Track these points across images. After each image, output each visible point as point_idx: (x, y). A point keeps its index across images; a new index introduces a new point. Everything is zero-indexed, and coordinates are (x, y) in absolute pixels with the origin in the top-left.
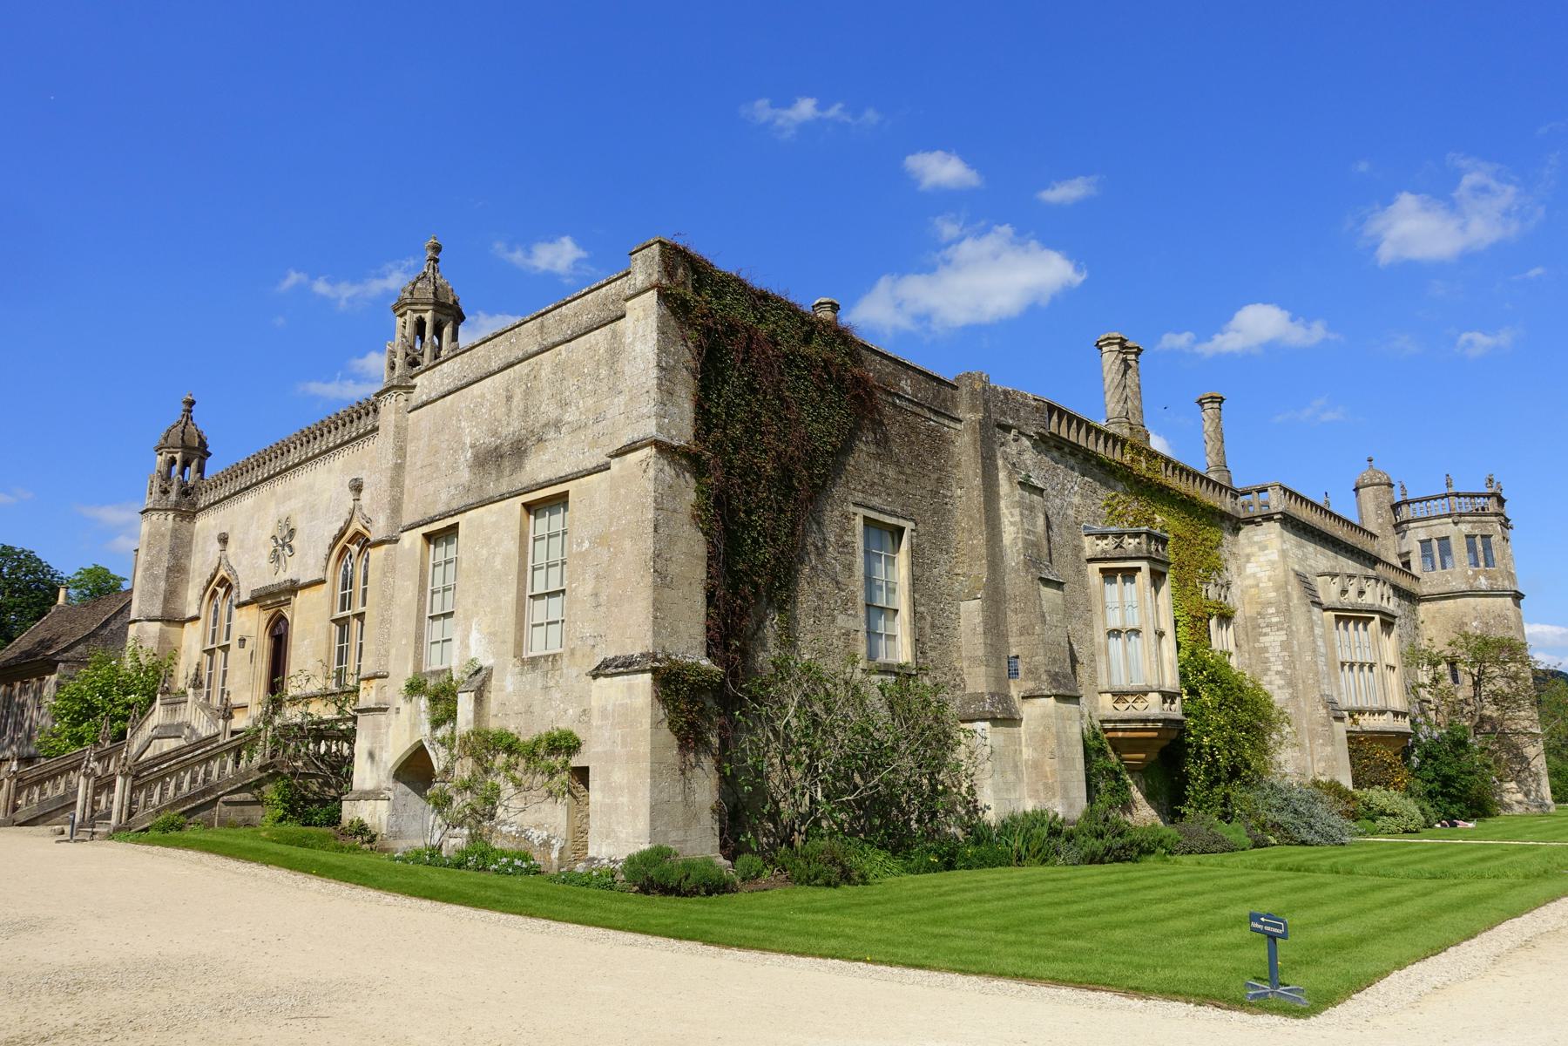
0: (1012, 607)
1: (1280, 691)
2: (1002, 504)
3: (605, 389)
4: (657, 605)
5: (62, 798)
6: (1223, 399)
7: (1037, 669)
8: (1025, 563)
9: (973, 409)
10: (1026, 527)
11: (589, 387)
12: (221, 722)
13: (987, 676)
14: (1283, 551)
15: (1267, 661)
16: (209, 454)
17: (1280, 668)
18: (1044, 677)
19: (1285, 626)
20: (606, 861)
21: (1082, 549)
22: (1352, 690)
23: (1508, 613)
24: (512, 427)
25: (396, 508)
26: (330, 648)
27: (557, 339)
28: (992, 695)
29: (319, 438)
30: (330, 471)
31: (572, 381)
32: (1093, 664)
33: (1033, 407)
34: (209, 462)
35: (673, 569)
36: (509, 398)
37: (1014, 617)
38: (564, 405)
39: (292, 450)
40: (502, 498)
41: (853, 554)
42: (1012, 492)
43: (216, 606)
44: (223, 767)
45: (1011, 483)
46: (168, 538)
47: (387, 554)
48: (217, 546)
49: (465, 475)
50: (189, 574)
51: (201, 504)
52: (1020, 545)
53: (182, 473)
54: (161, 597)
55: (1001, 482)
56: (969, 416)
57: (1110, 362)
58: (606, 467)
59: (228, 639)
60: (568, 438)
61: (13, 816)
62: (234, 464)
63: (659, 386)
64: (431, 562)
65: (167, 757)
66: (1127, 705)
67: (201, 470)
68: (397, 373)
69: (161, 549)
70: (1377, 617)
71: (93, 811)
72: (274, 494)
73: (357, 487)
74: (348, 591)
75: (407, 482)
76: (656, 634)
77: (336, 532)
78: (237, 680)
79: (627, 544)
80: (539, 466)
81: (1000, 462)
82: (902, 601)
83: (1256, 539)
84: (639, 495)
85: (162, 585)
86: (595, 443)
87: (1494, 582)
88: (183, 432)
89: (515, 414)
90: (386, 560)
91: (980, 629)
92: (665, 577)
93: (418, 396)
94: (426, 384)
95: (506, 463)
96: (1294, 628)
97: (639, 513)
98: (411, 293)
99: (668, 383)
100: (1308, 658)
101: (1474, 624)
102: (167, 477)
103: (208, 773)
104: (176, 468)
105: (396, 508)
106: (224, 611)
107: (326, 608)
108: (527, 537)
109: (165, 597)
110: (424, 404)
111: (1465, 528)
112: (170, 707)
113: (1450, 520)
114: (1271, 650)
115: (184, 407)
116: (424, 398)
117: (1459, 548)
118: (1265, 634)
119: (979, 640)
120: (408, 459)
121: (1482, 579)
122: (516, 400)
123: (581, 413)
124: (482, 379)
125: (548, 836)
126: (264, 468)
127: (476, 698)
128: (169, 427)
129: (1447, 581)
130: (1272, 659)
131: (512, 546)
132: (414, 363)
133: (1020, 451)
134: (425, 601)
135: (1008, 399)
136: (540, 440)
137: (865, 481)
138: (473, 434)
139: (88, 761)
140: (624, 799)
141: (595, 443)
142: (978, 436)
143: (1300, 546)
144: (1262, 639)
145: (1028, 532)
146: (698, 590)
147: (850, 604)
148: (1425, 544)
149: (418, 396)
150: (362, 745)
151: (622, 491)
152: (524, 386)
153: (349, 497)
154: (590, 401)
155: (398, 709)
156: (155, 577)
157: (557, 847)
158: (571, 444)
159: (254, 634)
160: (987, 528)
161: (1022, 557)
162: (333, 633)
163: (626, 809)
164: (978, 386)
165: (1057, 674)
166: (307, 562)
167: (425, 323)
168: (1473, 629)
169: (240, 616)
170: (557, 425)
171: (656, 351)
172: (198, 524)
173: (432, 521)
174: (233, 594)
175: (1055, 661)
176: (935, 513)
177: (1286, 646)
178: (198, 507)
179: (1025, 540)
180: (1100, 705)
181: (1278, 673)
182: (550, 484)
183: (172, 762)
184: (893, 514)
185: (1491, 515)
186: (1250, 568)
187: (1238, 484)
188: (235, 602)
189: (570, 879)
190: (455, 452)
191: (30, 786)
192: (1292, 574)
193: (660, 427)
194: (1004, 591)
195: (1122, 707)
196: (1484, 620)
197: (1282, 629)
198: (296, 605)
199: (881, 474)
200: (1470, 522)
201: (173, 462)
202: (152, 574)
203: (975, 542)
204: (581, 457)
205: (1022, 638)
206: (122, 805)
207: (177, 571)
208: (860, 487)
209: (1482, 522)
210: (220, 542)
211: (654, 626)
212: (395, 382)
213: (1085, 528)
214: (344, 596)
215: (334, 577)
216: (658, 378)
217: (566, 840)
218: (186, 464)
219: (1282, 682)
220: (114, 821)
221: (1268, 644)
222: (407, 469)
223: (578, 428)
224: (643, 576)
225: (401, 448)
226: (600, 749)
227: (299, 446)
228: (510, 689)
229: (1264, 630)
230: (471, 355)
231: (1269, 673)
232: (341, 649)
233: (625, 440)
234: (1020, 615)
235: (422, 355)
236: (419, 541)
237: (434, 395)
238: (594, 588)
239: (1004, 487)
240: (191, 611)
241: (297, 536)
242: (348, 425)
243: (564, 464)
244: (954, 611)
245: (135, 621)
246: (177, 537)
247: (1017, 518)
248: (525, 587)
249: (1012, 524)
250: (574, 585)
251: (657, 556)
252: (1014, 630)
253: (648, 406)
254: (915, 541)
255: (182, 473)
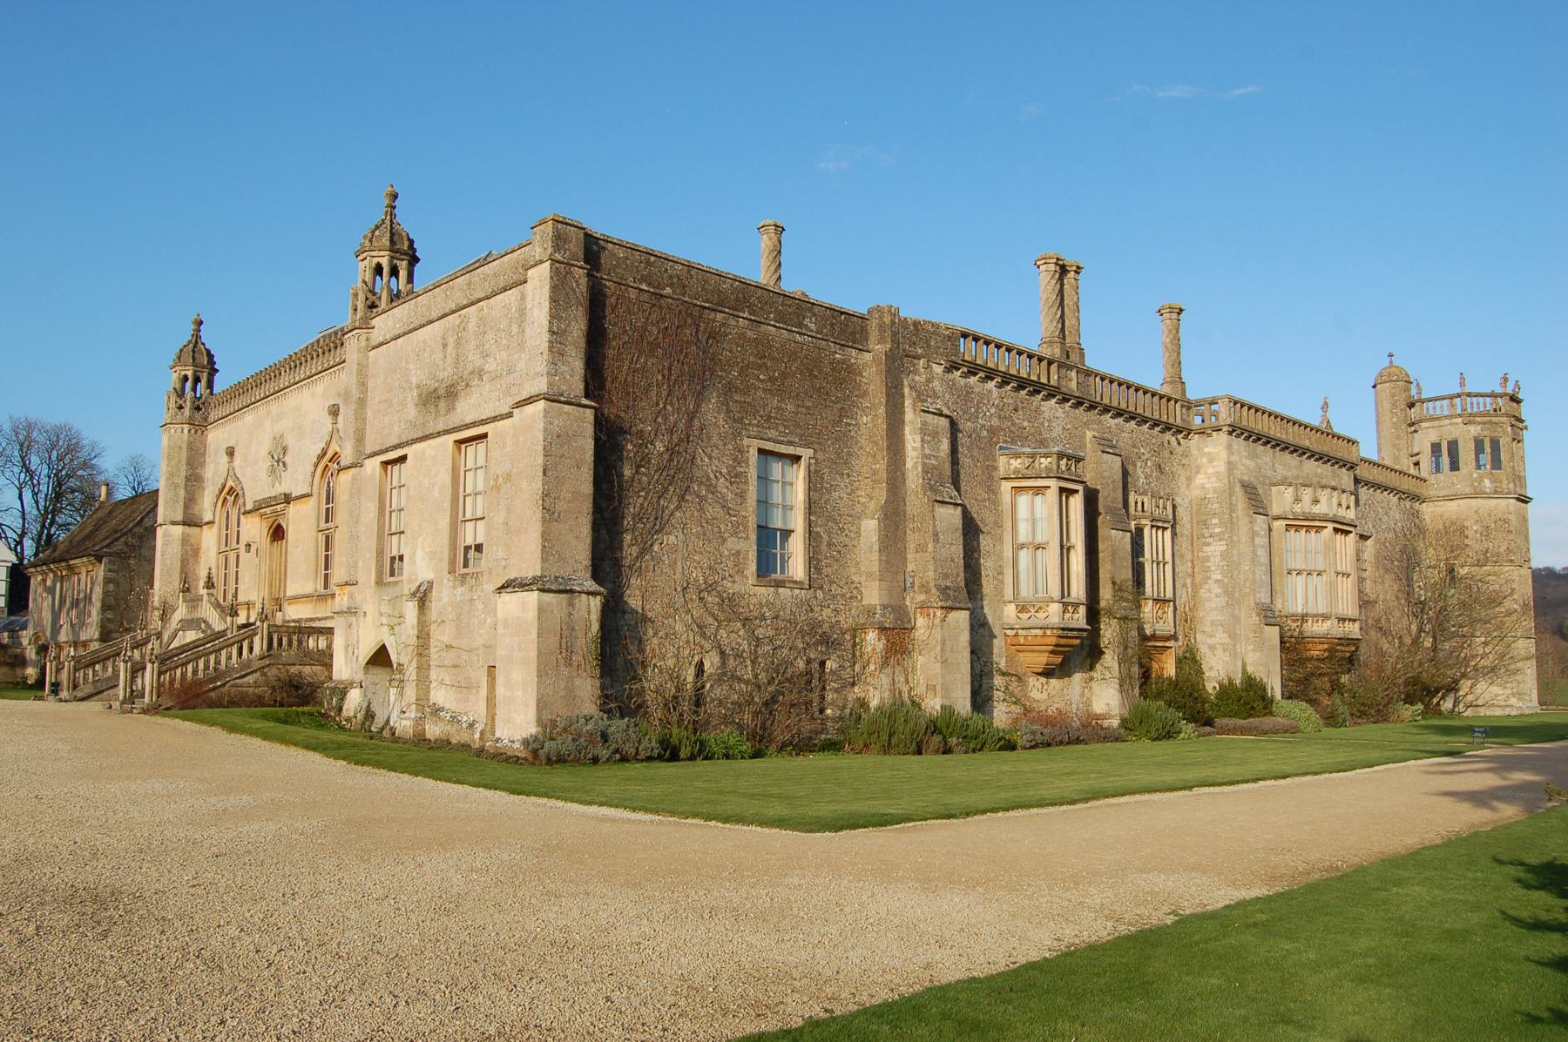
0: (911, 526)
1: (1217, 599)
2: (907, 430)
3: (516, 345)
4: (545, 537)
5: (109, 679)
6: (1181, 310)
7: (928, 583)
8: (923, 485)
9: (881, 340)
10: (927, 451)
11: (504, 342)
12: (229, 619)
13: (880, 589)
14: (1230, 463)
15: (1207, 570)
16: (217, 371)
17: (1219, 577)
18: (934, 590)
19: (1226, 536)
20: (506, 741)
21: (995, 468)
22: (1299, 596)
23: (1510, 516)
24: (447, 373)
25: (360, 439)
26: (317, 555)
27: (481, 295)
28: (885, 607)
29: (304, 364)
30: (313, 395)
31: (490, 335)
32: (1000, 577)
33: (945, 336)
34: (217, 377)
35: (561, 506)
36: (445, 346)
37: (913, 536)
38: (485, 355)
39: (283, 373)
40: (439, 434)
41: (746, 483)
42: (915, 419)
43: (228, 512)
44: (229, 658)
45: (915, 410)
46: (185, 450)
47: (354, 479)
48: (225, 458)
49: (412, 412)
50: (204, 482)
51: (211, 419)
52: (920, 469)
53: (194, 390)
54: (182, 503)
55: (906, 410)
56: (879, 347)
57: (1045, 283)
58: (510, 415)
59: (238, 543)
60: (488, 386)
61: (74, 693)
62: (245, 379)
63: (551, 349)
64: (389, 487)
65: (186, 648)
66: (1029, 614)
67: (210, 385)
68: (359, 316)
69: (180, 461)
70: (1331, 526)
71: (132, 691)
72: (269, 413)
73: (334, 412)
74: (331, 505)
75: (369, 413)
76: (544, 560)
77: (319, 452)
78: (246, 580)
79: (524, 485)
80: (469, 408)
81: (907, 390)
82: (798, 522)
83: (1206, 450)
84: (532, 443)
85: (182, 493)
86: (507, 392)
87: (1498, 485)
88: (194, 351)
89: (449, 360)
90: (352, 483)
91: (876, 547)
92: (553, 513)
93: (377, 336)
94: (384, 324)
95: (442, 404)
96: (1235, 538)
97: (532, 458)
98: (371, 241)
99: (558, 345)
100: (1247, 568)
101: (1475, 528)
102: (181, 394)
103: (218, 662)
104: (189, 385)
105: (360, 439)
106: (234, 518)
107: (313, 520)
108: (459, 470)
109: (185, 503)
110: (381, 344)
111: (1474, 430)
112: (190, 604)
113: (1460, 420)
114: (1212, 559)
115: (193, 327)
116: (381, 339)
117: (1466, 455)
118: (1208, 544)
119: (875, 556)
120: (369, 394)
121: (1487, 482)
122: (450, 348)
123: (498, 365)
124: (424, 326)
125: (474, 721)
126: (260, 389)
127: (419, 607)
128: (181, 346)
129: (1453, 483)
130: (1213, 568)
131: (445, 477)
132: (373, 306)
133: (930, 373)
134: (384, 520)
135: (918, 330)
136: (467, 385)
137: (761, 416)
138: (417, 376)
139: (126, 650)
140: (519, 693)
141: (507, 392)
142: (883, 367)
143: (1253, 456)
144: (1206, 549)
145: (929, 457)
146: (584, 522)
147: (741, 528)
148: (1436, 448)
149: (377, 336)
150: (338, 642)
151: (521, 439)
152: (456, 336)
153: (328, 420)
154: (504, 354)
155: (365, 613)
156: (177, 486)
157: (479, 729)
158: (491, 391)
159: (258, 540)
160: (888, 454)
161: (921, 480)
162: (320, 545)
163: (520, 701)
164: (887, 319)
165: (947, 587)
166: (296, 479)
167: (382, 268)
168: (1472, 532)
169: (247, 523)
170: (480, 373)
171: (548, 318)
172: (210, 437)
173: (387, 450)
174: (241, 501)
175: (946, 576)
176: (837, 439)
177: (1225, 556)
178: (209, 420)
179: (924, 465)
180: (1006, 613)
181: (1217, 581)
182: (474, 424)
183: (189, 653)
184: (790, 443)
185: (1502, 415)
186: (1200, 480)
187: (1192, 395)
188: (242, 510)
189: (481, 751)
190: (404, 390)
191: (87, 666)
192: (1238, 487)
193: (550, 385)
194: (905, 512)
195: (1025, 616)
196: (1485, 523)
197: (1223, 539)
198: (290, 517)
199: (779, 408)
200: (1479, 423)
201: (186, 378)
202: (173, 483)
203: (878, 466)
204: (497, 403)
205: (918, 554)
206: (126, 684)
207: (194, 480)
208: (755, 422)
209: (1490, 422)
210: (227, 454)
211: (542, 554)
212: (357, 325)
213: (1001, 448)
214: (328, 509)
215: (319, 489)
216: (550, 342)
217: (486, 724)
218: (197, 380)
219: (1220, 591)
220: (147, 699)
221: (1210, 554)
222: (369, 402)
223: (495, 378)
224: (535, 512)
225: (363, 384)
226: (503, 653)
227: (288, 370)
228: (446, 599)
229: (1207, 540)
230: (416, 302)
231: (1210, 581)
232: (327, 556)
233: (526, 393)
234: (917, 534)
235: (380, 298)
236: (378, 468)
237: (388, 337)
238: (506, 518)
239: (911, 417)
240: (208, 517)
241: (289, 453)
242: (327, 353)
243: (485, 409)
244: (855, 529)
245: (161, 525)
246: (192, 449)
247: (918, 445)
248: (457, 513)
249: (914, 449)
250: (491, 515)
251: (546, 495)
252: (912, 546)
253: (541, 366)
254: (812, 468)
255: (194, 390)
